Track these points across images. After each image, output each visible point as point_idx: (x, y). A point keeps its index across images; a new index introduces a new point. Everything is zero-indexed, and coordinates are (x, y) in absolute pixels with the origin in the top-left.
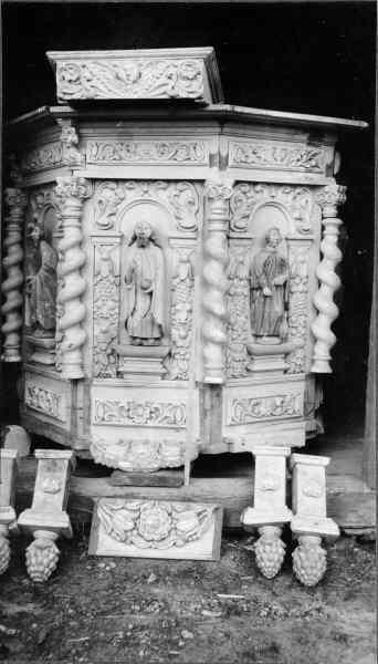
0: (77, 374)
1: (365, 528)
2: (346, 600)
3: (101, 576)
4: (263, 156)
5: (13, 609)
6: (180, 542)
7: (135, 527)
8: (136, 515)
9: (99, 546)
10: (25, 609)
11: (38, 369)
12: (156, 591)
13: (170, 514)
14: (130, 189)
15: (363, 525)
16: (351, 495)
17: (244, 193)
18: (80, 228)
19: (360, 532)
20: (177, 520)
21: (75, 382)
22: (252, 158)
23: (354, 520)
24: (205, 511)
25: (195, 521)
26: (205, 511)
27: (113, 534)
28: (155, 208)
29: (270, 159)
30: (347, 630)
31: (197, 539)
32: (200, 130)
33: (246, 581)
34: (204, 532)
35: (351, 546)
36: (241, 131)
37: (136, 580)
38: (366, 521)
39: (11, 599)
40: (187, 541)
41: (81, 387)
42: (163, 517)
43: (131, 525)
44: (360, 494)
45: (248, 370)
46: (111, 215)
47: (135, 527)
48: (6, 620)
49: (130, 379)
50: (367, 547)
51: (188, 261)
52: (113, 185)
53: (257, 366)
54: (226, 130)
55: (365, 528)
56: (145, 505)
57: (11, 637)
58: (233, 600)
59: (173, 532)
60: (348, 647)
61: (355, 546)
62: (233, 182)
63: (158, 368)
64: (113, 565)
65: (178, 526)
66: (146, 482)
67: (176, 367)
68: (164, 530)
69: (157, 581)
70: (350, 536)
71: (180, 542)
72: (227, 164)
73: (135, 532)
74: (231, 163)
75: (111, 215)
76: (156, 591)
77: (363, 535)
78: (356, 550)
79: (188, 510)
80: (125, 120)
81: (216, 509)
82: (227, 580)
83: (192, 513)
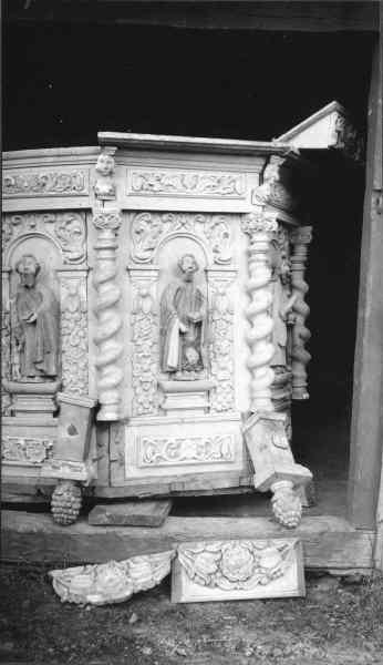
1: (350, 568)
6: (264, 580)
7: (219, 569)
8: (219, 556)
9: (184, 592)
12: (139, 631)
13: (252, 553)
15: (347, 565)
16: (336, 534)
18: (114, 259)
19: (345, 573)
20: (260, 558)
23: (339, 560)
24: (287, 546)
25: (278, 558)
26: (287, 546)
27: (197, 578)
29: (180, 187)
31: (282, 575)
32: (152, 161)
34: (287, 568)
35: (336, 586)
37: (116, 622)
38: (350, 562)
40: (272, 579)
42: (246, 556)
43: (213, 568)
44: (344, 534)
47: (219, 569)
50: (349, 588)
51: (111, 461)
52: (150, 217)
53: (171, 402)
55: (350, 568)
56: (225, 547)
59: (257, 571)
61: (339, 588)
65: (261, 564)
67: (218, 401)
68: (248, 568)
69: (139, 621)
71: (264, 580)
73: (219, 574)
76: (139, 631)
77: (347, 576)
78: (340, 591)
79: (269, 546)
81: (297, 543)
83: (273, 549)
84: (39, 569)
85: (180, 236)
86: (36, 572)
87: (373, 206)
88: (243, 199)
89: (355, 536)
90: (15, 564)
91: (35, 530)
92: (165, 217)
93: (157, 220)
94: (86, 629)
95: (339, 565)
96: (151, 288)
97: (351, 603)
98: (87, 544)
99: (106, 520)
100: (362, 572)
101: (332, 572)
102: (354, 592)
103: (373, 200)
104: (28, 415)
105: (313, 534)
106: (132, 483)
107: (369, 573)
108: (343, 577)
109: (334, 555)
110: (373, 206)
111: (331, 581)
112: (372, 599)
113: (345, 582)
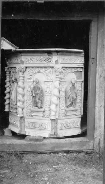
0: (22, 115)
2: (84, 167)
3: (24, 163)
4: (34, 60)
5: (2, 172)
10: (5, 171)
11: (13, 113)
14: (35, 69)
15: (87, 149)
17: (31, 69)
18: (24, 79)
19: (87, 151)
21: (21, 117)
22: (30, 61)
28: (40, 74)
30: (84, 173)
33: (60, 163)
36: (27, 54)
39: (2, 169)
41: (23, 119)
44: (86, 141)
45: (66, 115)
46: (31, 76)
48: (53, 168)
49: (34, 117)
52: (31, 68)
53: (68, 114)
54: (22, 54)
57: (3, 177)
58: (57, 168)
60: (85, 176)
62: (62, 67)
63: (42, 115)
64: (26, 161)
66: (33, 140)
70: (84, 152)
72: (24, 63)
74: (25, 62)
75: (31, 76)
77: (87, 152)
80: (58, 52)
82: (55, 163)
84: (12, 153)
85: (37, 72)
86: (12, 154)
87: (91, 62)
88: (53, 63)
89: (89, 142)
90: (6, 152)
91: (11, 143)
92: (68, 68)
93: (33, 69)
94: (24, 167)
95: (85, 149)
96: (29, 86)
97: (89, 158)
98: (24, 146)
99: (29, 140)
100: (91, 151)
101: (84, 151)
102: (89, 155)
103: (91, 60)
104: (39, 117)
105: (79, 142)
106: (95, 132)
107: (93, 151)
108: (87, 152)
109: (84, 147)
110: (91, 62)
111: (84, 153)
112: (94, 157)
113: (87, 153)
